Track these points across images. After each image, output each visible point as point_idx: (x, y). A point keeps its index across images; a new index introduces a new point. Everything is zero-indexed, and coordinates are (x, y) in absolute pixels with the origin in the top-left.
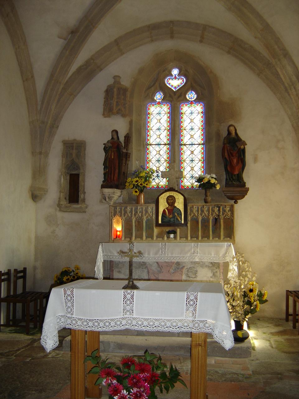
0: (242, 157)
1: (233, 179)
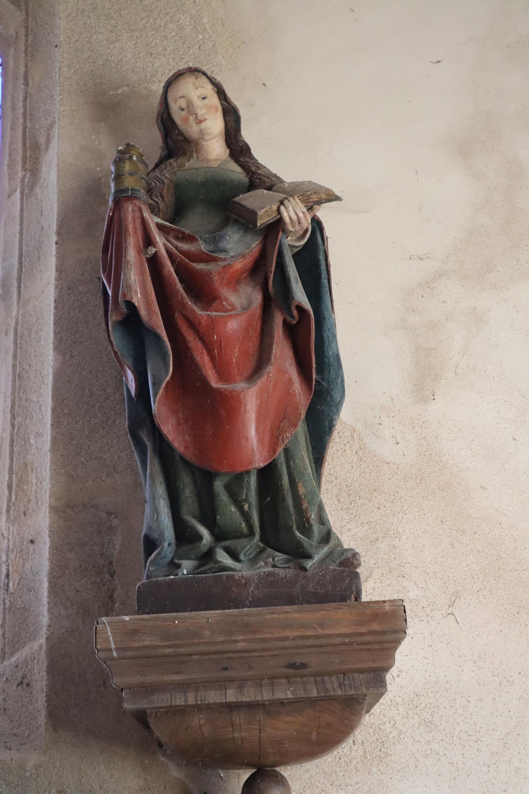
0: (300, 295)
1: (219, 536)
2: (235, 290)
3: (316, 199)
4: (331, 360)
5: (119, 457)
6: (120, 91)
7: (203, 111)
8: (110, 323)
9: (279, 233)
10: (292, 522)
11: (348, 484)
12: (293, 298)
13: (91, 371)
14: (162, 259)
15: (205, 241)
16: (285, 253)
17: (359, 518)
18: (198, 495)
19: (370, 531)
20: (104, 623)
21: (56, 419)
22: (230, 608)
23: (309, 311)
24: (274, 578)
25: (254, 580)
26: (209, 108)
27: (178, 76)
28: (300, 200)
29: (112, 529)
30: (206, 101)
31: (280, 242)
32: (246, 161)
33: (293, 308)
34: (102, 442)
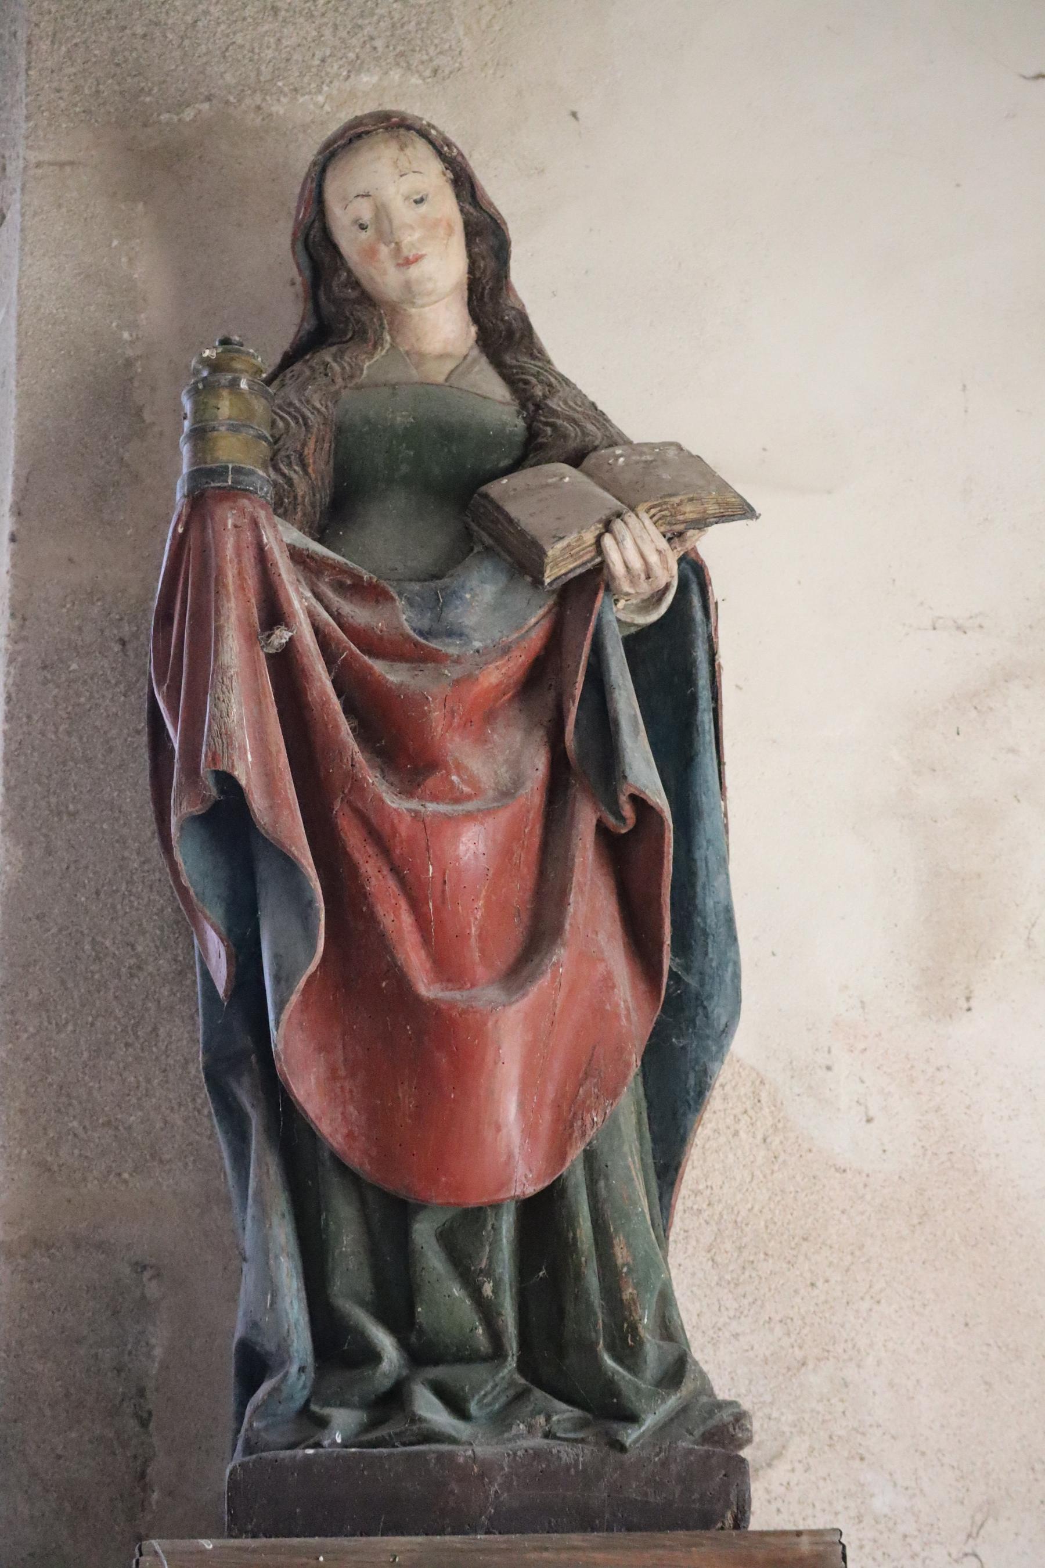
0: (642, 770)
1: (420, 1354)
2: (482, 740)
4: (712, 920)
5: (166, 1122)
7: (417, 235)
8: (174, 820)
9: (596, 594)
10: (596, 1332)
11: (739, 1219)
12: (625, 777)
13: (98, 893)
14: (305, 660)
15: (410, 603)
16: (610, 650)
17: (762, 1306)
18: (373, 1251)
19: (786, 1342)
20: (156, 1552)
21: (8, 1017)
22: (441, 1532)
23: (662, 811)
24: (548, 1466)
25: (503, 1469)
26: (431, 226)
27: (353, 137)
28: (651, 518)
29: (144, 1307)
30: (423, 208)
31: (600, 619)
32: (520, 367)
33: (623, 799)
34: (124, 1081)
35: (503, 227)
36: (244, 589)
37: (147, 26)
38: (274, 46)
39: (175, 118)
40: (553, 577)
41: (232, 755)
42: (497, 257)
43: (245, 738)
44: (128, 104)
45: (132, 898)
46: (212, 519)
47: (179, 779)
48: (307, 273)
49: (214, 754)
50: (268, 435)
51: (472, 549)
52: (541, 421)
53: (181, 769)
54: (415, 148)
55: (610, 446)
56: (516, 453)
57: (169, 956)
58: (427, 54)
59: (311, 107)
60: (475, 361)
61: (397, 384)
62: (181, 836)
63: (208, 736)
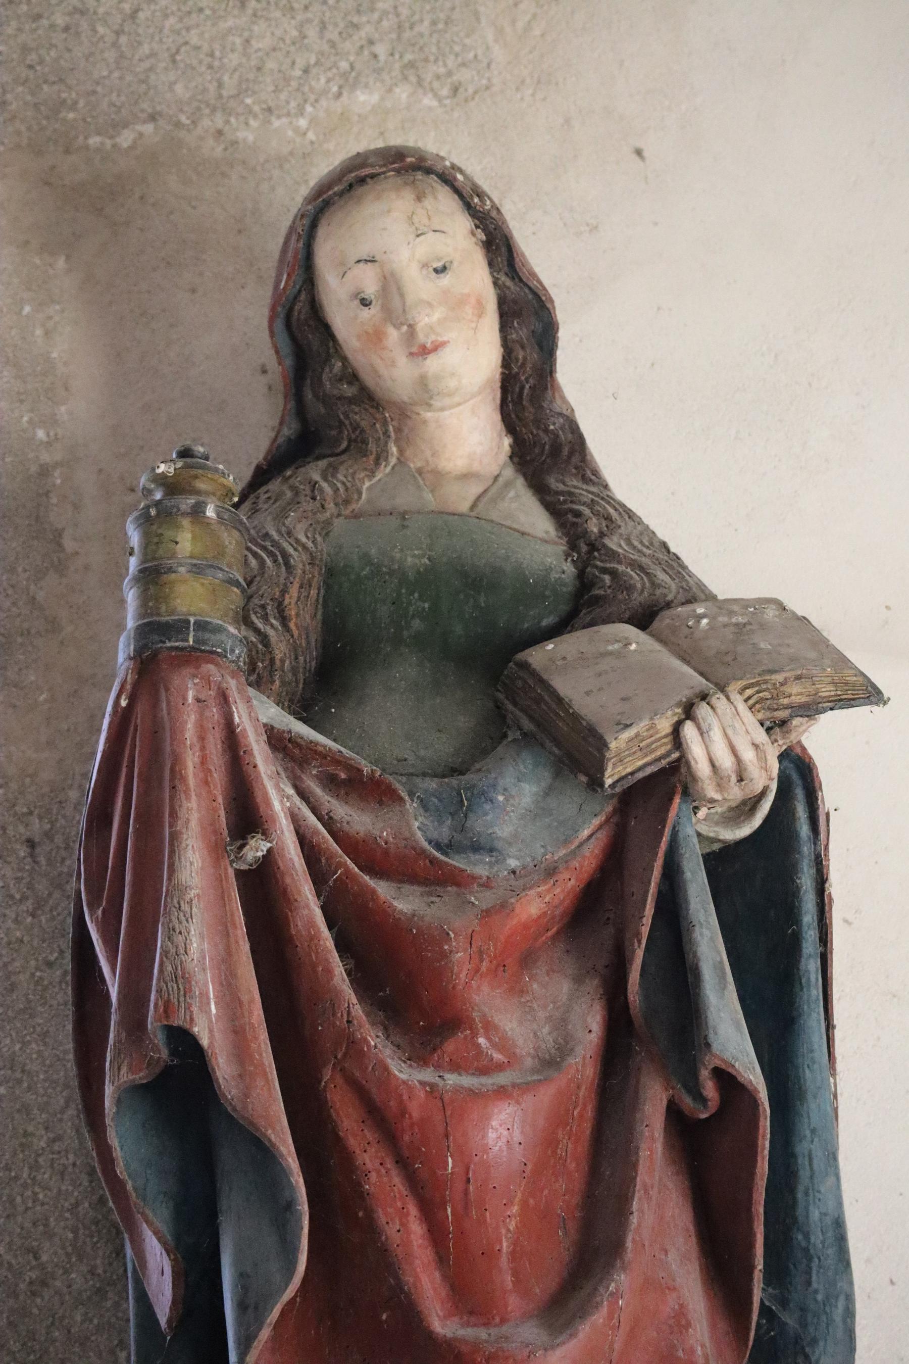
0: (730, 1035)
2: (517, 990)
3: (803, 699)
4: (816, 1238)
6: (126, 139)
7: (437, 316)
9: (671, 800)
12: (708, 1045)
14: (288, 880)
16: (688, 875)
26: (455, 303)
27: (354, 181)
28: (746, 701)
30: (445, 280)
32: (571, 494)
33: (705, 1074)
35: (549, 305)
36: (206, 783)
37: (70, 14)
38: (239, 48)
39: (108, 143)
40: (616, 777)
41: (190, 1005)
42: (541, 347)
43: (206, 983)
44: (44, 122)
45: (37, 1189)
46: (167, 690)
47: (118, 1034)
48: (289, 362)
49: (167, 1004)
50: (241, 580)
51: (505, 736)
52: (596, 567)
53: (120, 1023)
54: (435, 198)
55: (688, 602)
56: (564, 608)
57: (84, 1269)
58: (445, 65)
59: (290, 133)
60: (508, 484)
61: (405, 512)
62: (117, 1112)
63: (159, 980)
